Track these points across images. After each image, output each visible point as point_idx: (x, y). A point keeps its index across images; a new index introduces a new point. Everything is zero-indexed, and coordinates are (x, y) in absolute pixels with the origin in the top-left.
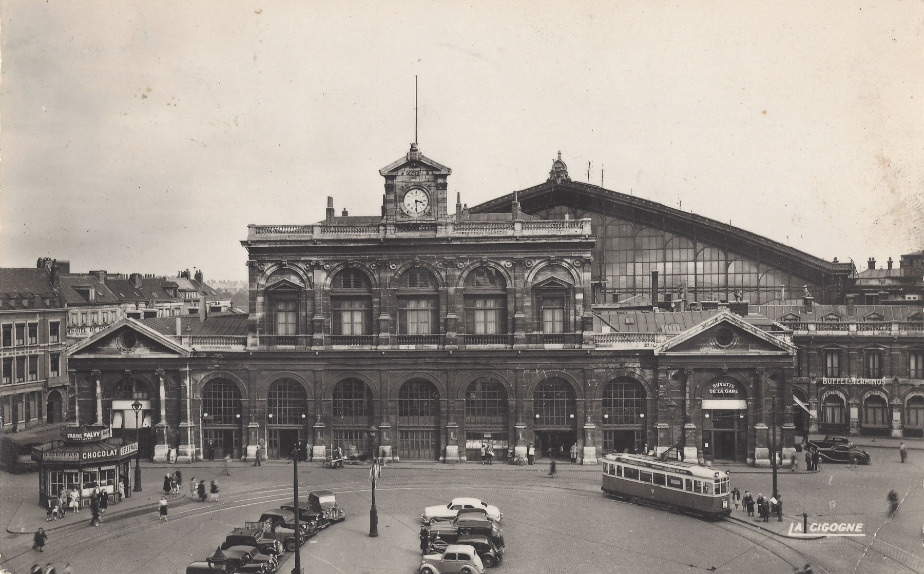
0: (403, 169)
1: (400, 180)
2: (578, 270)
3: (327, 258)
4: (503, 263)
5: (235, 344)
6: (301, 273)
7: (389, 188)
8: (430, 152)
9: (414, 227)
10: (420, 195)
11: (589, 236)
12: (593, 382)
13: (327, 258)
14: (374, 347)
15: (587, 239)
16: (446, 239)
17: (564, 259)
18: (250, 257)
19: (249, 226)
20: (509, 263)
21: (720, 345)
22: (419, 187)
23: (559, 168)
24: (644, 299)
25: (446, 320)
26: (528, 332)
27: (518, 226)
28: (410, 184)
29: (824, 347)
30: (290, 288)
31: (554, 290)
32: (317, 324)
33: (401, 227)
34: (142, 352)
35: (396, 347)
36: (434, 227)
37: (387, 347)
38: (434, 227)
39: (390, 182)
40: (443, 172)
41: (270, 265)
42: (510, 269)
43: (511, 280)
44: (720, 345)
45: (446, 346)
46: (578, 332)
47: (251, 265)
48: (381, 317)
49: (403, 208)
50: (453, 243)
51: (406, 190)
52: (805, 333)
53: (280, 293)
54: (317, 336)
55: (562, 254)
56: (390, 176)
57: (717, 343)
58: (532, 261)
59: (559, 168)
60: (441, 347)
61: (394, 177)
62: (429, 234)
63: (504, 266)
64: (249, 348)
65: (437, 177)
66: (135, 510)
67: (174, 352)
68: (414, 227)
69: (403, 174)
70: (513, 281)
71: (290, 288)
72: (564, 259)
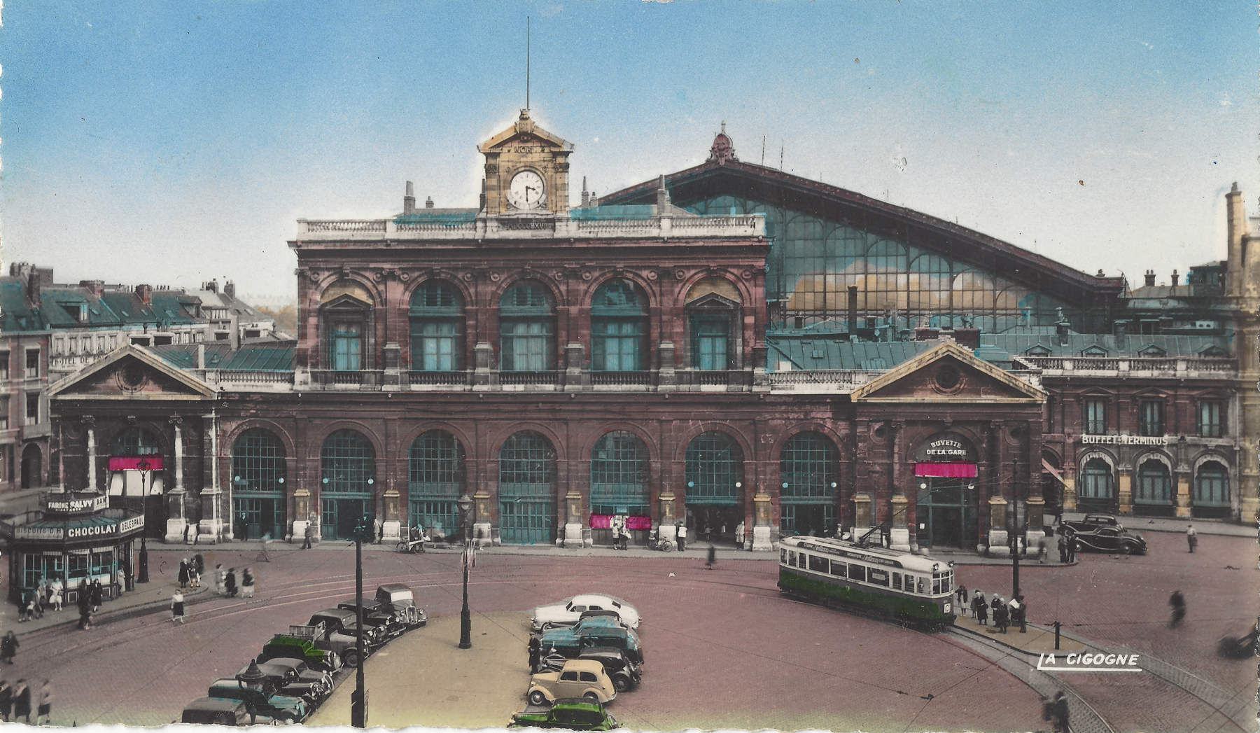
0: (509, 145)
1: (507, 158)
3: (404, 265)
4: (645, 273)
6: (369, 285)
7: (490, 170)
10: (532, 180)
12: (768, 438)
13: (404, 265)
14: (468, 387)
16: (567, 240)
18: (300, 263)
19: (299, 221)
20: (653, 274)
21: (941, 389)
22: (531, 168)
25: (567, 351)
26: (677, 368)
30: (354, 305)
34: (151, 393)
35: (498, 387)
38: (551, 223)
39: (492, 161)
40: (566, 149)
41: (327, 274)
44: (941, 389)
45: (567, 387)
46: (748, 369)
47: (301, 275)
51: (513, 172)
53: (340, 312)
54: (390, 371)
55: (725, 262)
57: (938, 386)
58: (686, 271)
62: (545, 234)
63: (645, 277)
64: (298, 387)
65: (555, 155)
67: (194, 392)
68: (525, 223)
69: (509, 151)
72: (729, 269)
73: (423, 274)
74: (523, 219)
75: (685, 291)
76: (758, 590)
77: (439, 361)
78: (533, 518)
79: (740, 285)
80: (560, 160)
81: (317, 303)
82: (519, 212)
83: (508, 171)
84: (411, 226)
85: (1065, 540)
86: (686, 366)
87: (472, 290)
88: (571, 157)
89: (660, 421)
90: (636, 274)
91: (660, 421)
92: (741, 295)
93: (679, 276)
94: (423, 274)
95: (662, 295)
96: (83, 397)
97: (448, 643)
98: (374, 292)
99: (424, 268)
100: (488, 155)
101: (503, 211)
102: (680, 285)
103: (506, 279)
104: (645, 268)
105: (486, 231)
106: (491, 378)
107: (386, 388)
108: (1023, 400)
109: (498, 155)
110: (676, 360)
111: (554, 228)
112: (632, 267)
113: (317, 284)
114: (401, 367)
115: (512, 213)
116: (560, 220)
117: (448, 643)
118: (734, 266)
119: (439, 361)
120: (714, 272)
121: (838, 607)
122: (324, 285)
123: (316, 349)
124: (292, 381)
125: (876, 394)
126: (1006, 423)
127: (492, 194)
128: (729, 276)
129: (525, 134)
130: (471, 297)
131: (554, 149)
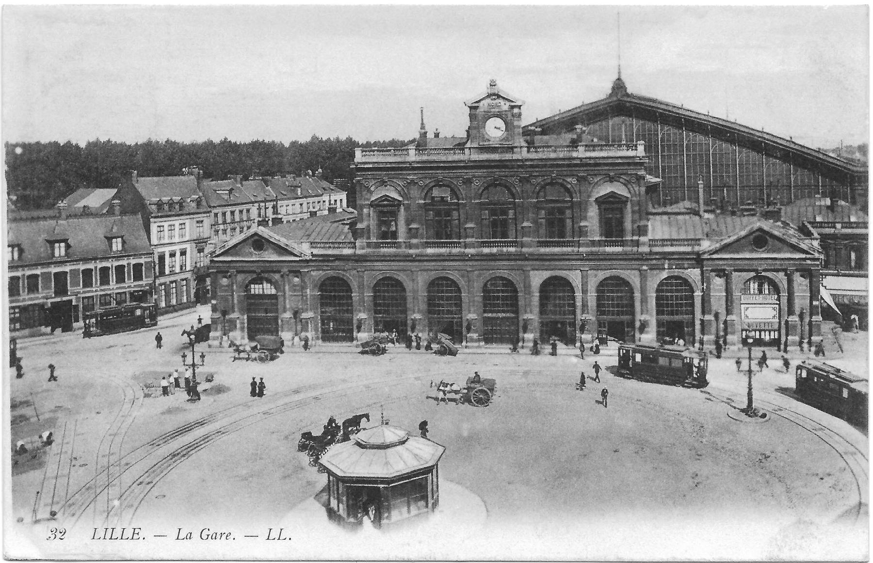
2: (634, 185)
4: (569, 180)
5: (430, 247)
7: (472, 117)
9: (493, 150)
10: (499, 122)
11: (643, 157)
15: (640, 159)
17: (622, 176)
22: (499, 115)
23: (619, 86)
24: (112, 437)
25: (522, 228)
27: (581, 149)
28: (490, 114)
29: (850, 243)
31: (613, 203)
32: (413, 231)
33: (482, 149)
34: (271, 256)
35: (480, 249)
36: (511, 149)
37: (531, 250)
39: (473, 111)
42: (576, 185)
43: (576, 193)
50: (628, 317)
51: (488, 116)
52: (832, 231)
59: (619, 86)
60: (519, 249)
61: (476, 108)
62: (508, 156)
65: (512, 107)
66: (809, 152)
68: (493, 150)
70: (578, 195)
71: (392, 201)
72: (622, 176)
76: (612, 268)
77: (263, 291)
79: (629, 186)
82: (491, 143)
90: (564, 180)
93: (591, 181)
96: (229, 259)
100: (471, 108)
106: (476, 244)
107: (411, 251)
111: (699, 245)
118: (624, 174)
119: (263, 291)
121: (590, 190)
124: (354, 247)
125: (716, 252)
126: (797, 270)
127: (473, 132)
128: (621, 180)
129: (494, 94)
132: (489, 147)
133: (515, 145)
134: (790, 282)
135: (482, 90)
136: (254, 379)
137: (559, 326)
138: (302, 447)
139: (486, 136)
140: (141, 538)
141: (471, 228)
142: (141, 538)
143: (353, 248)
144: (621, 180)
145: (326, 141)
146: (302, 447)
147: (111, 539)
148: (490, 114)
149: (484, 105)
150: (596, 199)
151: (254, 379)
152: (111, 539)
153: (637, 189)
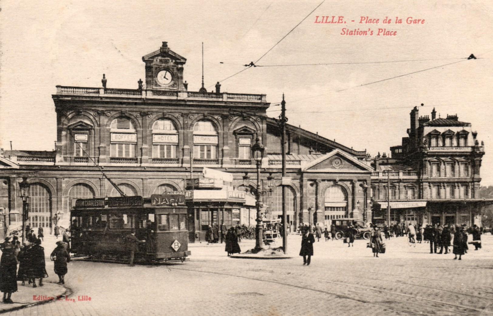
4: (216, 117)
6: (91, 117)
7: (148, 69)
8: (174, 47)
9: (164, 93)
10: (162, 73)
16: (183, 101)
19: (57, 87)
22: (167, 69)
30: (85, 126)
40: (182, 61)
48: (81, 145)
49: (157, 81)
51: (159, 70)
56: (148, 61)
68: (164, 93)
73: (117, 113)
74: (163, 91)
75: (233, 125)
78: (33, 224)
79: (256, 124)
80: (180, 66)
81: (66, 125)
82: (161, 87)
83: (156, 68)
84: (195, 95)
85: (402, 220)
86: (234, 157)
87: (140, 121)
88: (184, 66)
89: (57, 178)
91: (57, 178)
92: (256, 127)
94: (117, 113)
95: (223, 126)
97: (301, 265)
98: (94, 121)
99: (118, 111)
101: (154, 87)
102: (231, 123)
103: (155, 117)
104: (217, 114)
105: (146, 95)
108: (8, 167)
109: (152, 61)
110: (229, 155)
112: (210, 114)
113: (66, 117)
114: (149, 156)
115: (158, 88)
116: (180, 92)
117: (301, 265)
120: (246, 117)
122: (70, 116)
123: (66, 146)
130: (181, 125)
131: (177, 61)
132: (160, 91)
133: (180, 90)
134: (353, 188)
135: (156, 47)
136: (318, 241)
137: (152, 231)
138: (163, 43)
139: (158, 83)
140: (344, 23)
141: (146, 148)
142: (344, 23)
143: (53, 161)
144: (251, 119)
145: (41, 247)
146: (163, 43)
147: (326, 22)
148: (161, 67)
149: (157, 61)
150: (234, 131)
151: (318, 241)
152: (326, 22)
153: (261, 126)
